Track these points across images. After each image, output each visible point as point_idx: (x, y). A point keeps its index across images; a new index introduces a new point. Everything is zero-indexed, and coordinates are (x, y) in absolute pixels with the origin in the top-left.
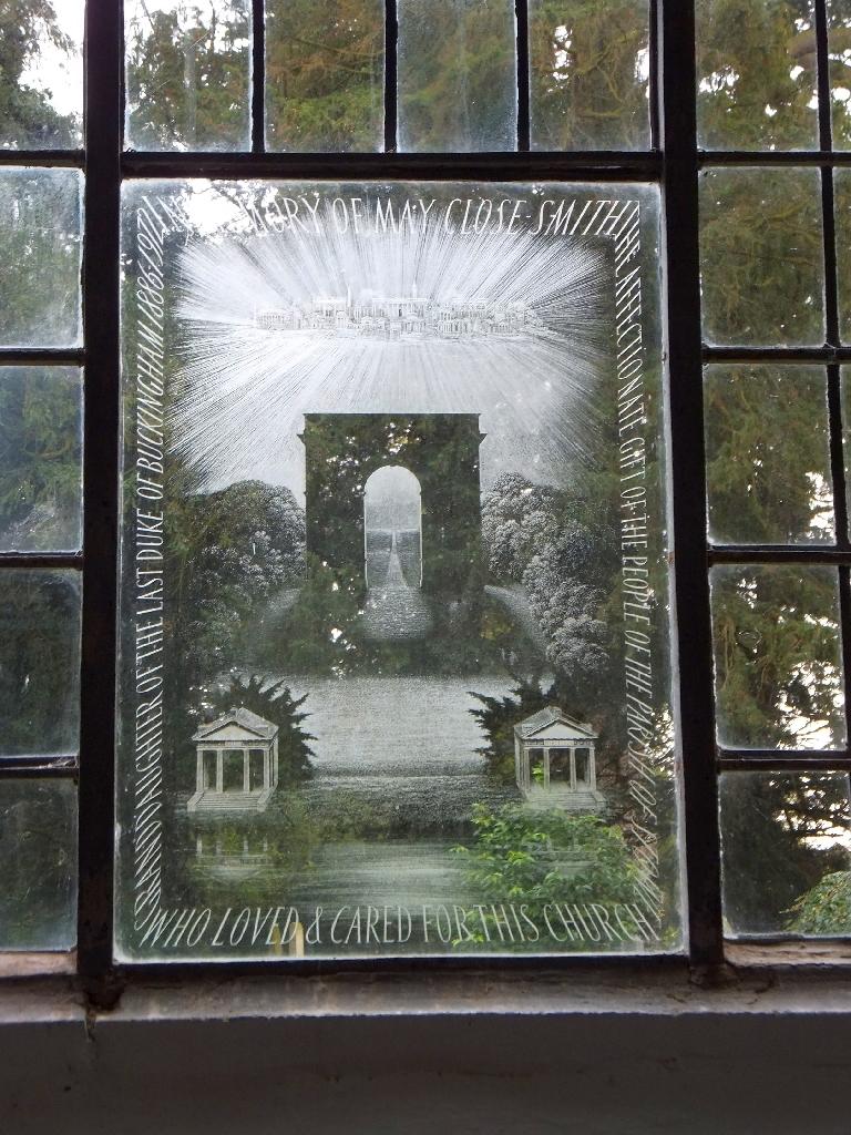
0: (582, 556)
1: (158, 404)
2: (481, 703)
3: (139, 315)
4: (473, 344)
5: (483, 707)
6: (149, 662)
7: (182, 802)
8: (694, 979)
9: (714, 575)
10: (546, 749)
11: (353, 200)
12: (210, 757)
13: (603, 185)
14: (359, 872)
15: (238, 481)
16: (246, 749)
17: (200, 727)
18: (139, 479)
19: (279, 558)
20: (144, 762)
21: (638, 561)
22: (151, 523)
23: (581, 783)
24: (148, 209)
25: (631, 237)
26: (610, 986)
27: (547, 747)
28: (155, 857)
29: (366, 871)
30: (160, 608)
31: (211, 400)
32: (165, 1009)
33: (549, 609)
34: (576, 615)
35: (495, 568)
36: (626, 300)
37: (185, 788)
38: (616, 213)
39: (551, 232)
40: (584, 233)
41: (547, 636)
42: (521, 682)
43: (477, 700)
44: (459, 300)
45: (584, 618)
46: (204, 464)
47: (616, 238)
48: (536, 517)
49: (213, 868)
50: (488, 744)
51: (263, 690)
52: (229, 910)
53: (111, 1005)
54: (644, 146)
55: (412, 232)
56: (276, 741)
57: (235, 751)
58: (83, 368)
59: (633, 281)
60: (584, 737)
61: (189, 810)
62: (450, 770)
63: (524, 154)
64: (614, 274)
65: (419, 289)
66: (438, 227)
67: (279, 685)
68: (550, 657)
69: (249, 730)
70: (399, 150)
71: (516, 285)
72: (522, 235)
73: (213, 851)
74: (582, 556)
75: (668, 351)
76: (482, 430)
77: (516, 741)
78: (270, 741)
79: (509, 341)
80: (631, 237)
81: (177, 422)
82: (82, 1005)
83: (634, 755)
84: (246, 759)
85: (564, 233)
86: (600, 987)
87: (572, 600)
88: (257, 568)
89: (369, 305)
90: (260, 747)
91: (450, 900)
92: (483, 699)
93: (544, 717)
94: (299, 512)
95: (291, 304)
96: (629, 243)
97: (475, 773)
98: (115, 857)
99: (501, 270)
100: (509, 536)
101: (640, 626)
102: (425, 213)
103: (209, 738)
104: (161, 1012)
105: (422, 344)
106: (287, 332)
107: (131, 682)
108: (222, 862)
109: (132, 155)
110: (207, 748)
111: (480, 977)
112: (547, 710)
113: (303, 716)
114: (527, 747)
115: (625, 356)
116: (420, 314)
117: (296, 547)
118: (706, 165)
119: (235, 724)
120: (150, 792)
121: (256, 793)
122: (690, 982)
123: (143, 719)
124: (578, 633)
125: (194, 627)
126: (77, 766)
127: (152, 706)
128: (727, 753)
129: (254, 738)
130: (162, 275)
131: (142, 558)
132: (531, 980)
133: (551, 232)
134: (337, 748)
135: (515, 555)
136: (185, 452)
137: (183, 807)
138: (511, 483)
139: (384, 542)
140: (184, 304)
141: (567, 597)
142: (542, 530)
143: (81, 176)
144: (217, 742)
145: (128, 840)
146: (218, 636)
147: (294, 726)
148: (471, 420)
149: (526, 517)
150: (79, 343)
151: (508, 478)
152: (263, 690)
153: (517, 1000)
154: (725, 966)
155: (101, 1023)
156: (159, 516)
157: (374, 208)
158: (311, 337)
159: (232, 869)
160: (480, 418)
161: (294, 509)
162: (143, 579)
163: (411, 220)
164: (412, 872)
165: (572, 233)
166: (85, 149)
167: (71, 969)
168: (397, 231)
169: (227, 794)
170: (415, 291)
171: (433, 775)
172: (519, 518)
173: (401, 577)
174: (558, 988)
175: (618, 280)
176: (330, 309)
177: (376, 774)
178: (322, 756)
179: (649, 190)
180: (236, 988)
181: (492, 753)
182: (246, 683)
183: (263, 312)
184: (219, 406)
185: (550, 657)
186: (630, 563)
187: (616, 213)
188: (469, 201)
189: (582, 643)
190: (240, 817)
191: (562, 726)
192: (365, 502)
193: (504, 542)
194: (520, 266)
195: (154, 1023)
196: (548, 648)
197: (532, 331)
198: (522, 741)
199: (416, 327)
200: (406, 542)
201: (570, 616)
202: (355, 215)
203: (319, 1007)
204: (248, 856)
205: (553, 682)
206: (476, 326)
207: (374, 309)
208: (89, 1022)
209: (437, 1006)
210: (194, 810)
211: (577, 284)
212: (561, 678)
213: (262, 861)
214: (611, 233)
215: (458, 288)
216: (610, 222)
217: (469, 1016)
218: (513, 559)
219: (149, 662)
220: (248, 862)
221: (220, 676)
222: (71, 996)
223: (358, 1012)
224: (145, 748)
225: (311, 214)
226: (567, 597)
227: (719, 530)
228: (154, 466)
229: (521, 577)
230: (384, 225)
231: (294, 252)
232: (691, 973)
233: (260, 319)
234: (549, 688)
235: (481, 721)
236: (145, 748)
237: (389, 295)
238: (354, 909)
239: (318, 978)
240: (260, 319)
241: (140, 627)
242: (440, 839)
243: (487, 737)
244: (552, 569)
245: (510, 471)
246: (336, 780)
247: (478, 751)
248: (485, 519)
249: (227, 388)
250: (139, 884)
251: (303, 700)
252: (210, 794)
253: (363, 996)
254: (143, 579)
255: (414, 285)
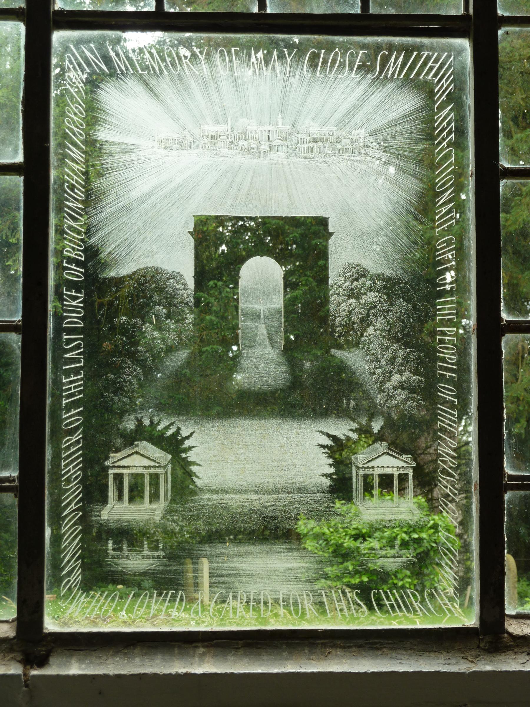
0: (406, 327)
1: (81, 206)
2: (327, 439)
3: (65, 136)
4: (325, 162)
5: (329, 442)
6: (75, 404)
7: (97, 511)
8: (482, 645)
9: (505, 343)
10: (376, 474)
11: (233, 49)
12: (119, 478)
13: (426, 41)
14: (232, 565)
15: (142, 266)
16: (146, 472)
17: (111, 455)
18: (65, 265)
19: (173, 326)
20: (68, 481)
21: (449, 331)
22: (74, 298)
23: (402, 499)
24: (74, 55)
25: (447, 80)
26: (419, 650)
27: (376, 473)
28: (76, 552)
29: (238, 565)
30: (82, 364)
31: (122, 203)
32: (83, 666)
33: (380, 367)
34: (401, 373)
35: (340, 336)
36: (443, 129)
37: (98, 501)
38: (435, 62)
39: (386, 76)
40: (411, 77)
41: (379, 388)
42: (358, 423)
43: (325, 437)
44: (315, 128)
45: (407, 374)
46: (116, 253)
47: (436, 81)
48: (370, 297)
49: (121, 561)
50: (332, 470)
51: (160, 428)
52: (64, 368)
53: (42, 663)
54: (458, 11)
55: (279, 75)
56: (169, 467)
57: (137, 474)
58: (22, 178)
59: (448, 115)
60: (405, 465)
61: (102, 518)
62: (302, 490)
63: (365, 15)
64: (434, 109)
65: (283, 118)
66: (298, 71)
67: (172, 424)
68: (380, 404)
69: (148, 458)
70: (269, 11)
71: (358, 118)
72: (364, 77)
73: (120, 549)
74: (406, 327)
75: (474, 170)
76: (331, 230)
77: (354, 468)
78: (165, 467)
79: (353, 160)
80: (447, 80)
81: (94, 221)
82: (20, 662)
83: (444, 479)
84: (147, 480)
85: (396, 77)
86: (412, 651)
87: (398, 360)
88: (156, 334)
89: (245, 131)
90: (157, 471)
91: (301, 587)
92: (328, 435)
93: (375, 450)
94: (189, 291)
95: (184, 129)
96: (445, 86)
97: (322, 492)
98: (46, 552)
99: (347, 105)
100: (350, 312)
101: (449, 381)
102: (289, 60)
103: (116, 464)
104: (80, 668)
105: (285, 162)
106: (180, 151)
107: (57, 420)
108: (127, 557)
109: (61, 12)
110: (117, 471)
111: (322, 644)
112: (377, 445)
113: (190, 448)
114: (361, 473)
115: (442, 172)
116: (284, 138)
117: (186, 318)
118: (505, 26)
119: (137, 453)
120: (73, 504)
121: (154, 505)
122: (479, 647)
123: (68, 448)
124: (402, 386)
125: (107, 379)
126: (16, 483)
127: (74, 439)
128: (511, 477)
129: (153, 464)
130: (84, 106)
131: (179, 595)
132: (360, 646)
133: (386, 76)
134: (216, 472)
135: (355, 326)
136: (101, 244)
137: (98, 516)
138: (353, 270)
139: (255, 316)
140: (101, 128)
141: (394, 358)
142: (375, 307)
143: (22, 28)
144: (124, 467)
145: (57, 539)
146: (126, 386)
147: (184, 455)
148: (323, 222)
149: (364, 296)
150: (20, 158)
151: (353, 266)
152: (160, 428)
153: (349, 661)
154: (506, 635)
155: (34, 676)
156: (81, 293)
157: (249, 56)
158: (199, 155)
159: (135, 562)
160: (329, 220)
161: (185, 289)
162: (69, 341)
163: (278, 65)
164: (272, 566)
165: (402, 77)
166: (25, 7)
167: (12, 634)
168: (266, 73)
169: (132, 506)
170: (280, 120)
171: (289, 493)
172: (358, 297)
173: (267, 343)
174: (381, 652)
175: (437, 114)
176: (214, 134)
177: (246, 492)
178: (204, 478)
179: (461, 45)
180: (137, 651)
181: (334, 477)
182: (146, 422)
183: (163, 136)
184: (127, 209)
185: (380, 404)
186: (443, 333)
187: (435, 62)
188: (323, 51)
189: (405, 394)
190: (142, 524)
191: (388, 457)
192: (240, 283)
193: (347, 316)
194: (363, 99)
195: (74, 676)
196: (379, 397)
197: (371, 153)
198: (358, 468)
199: (281, 149)
200: (271, 315)
201: (396, 373)
202: (235, 61)
203: (200, 666)
204: (147, 552)
205: (382, 423)
206: (327, 148)
207: (248, 134)
208: (25, 675)
209: (289, 666)
210: (106, 518)
211: (405, 116)
212: (388, 419)
213: (158, 557)
214: (432, 77)
215: (313, 119)
216: (431, 68)
217: (313, 674)
218: (353, 328)
219: (75, 404)
220: (148, 558)
221: (127, 417)
222: (12, 655)
223: (229, 671)
224: (69, 471)
225: (200, 60)
226: (394, 358)
227: (510, 310)
228: (76, 254)
229: (359, 343)
230: (257, 69)
231: (187, 88)
232: (480, 640)
233: (160, 142)
234: (379, 428)
235: (326, 453)
236: (69, 471)
237: (260, 124)
238: (228, 592)
239: (200, 645)
240: (160, 142)
241: (65, 379)
242: (293, 541)
243: (331, 465)
244: (383, 337)
245: (353, 261)
246: (215, 496)
247: (324, 475)
248: (332, 298)
249: (135, 194)
250: (64, 572)
251: (191, 435)
252: (119, 506)
253: (232, 658)
254: (69, 341)
255: (280, 116)
